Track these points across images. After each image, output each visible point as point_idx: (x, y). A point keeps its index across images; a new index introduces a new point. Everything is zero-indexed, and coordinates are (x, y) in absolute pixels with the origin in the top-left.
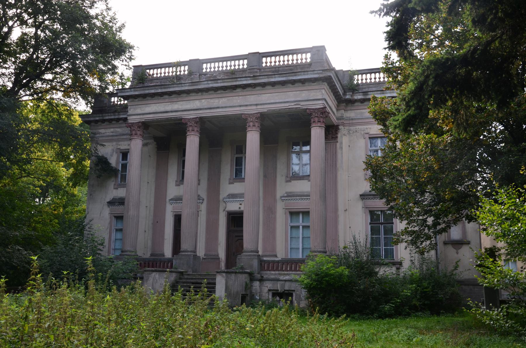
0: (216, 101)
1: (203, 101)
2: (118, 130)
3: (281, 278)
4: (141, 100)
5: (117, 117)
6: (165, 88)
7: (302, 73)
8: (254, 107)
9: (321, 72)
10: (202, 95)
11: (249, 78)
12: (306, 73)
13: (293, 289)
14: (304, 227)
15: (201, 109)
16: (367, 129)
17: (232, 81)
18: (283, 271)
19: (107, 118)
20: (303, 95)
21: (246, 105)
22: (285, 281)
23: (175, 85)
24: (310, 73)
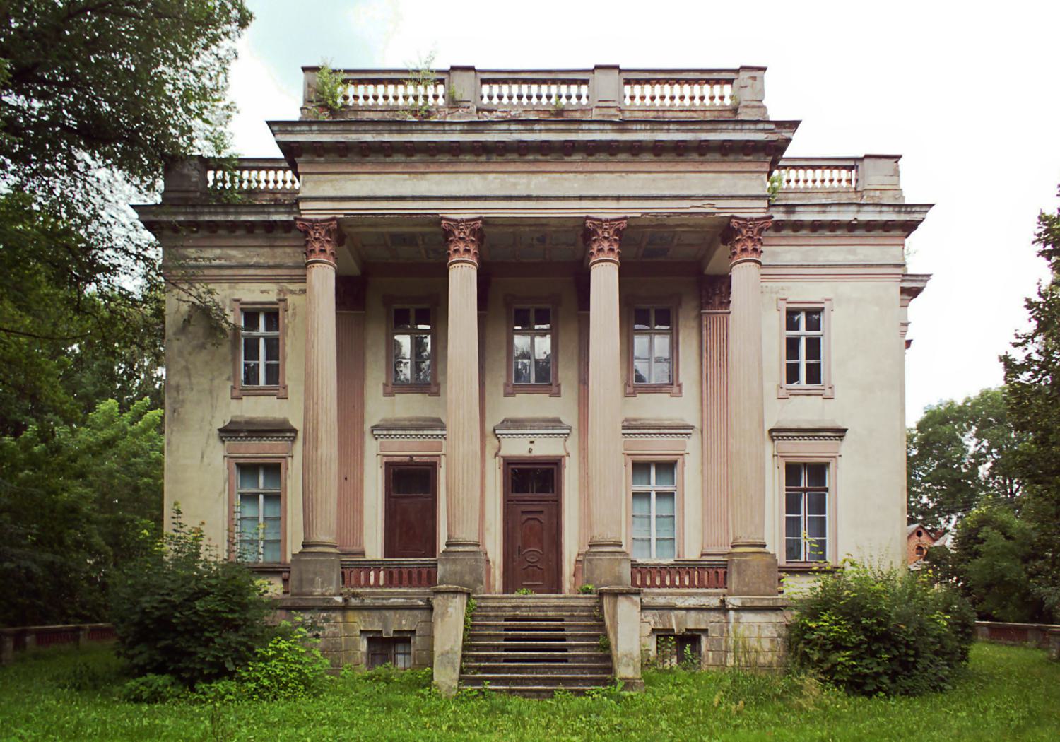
0: (523, 179)
1: (491, 176)
2: (233, 252)
3: (680, 602)
4: (334, 162)
5: (231, 218)
6: (400, 132)
7: (731, 127)
8: (613, 204)
9: (772, 127)
10: (488, 161)
11: (608, 127)
12: (739, 127)
13: (703, 627)
14: (659, 494)
15: (485, 198)
16: (782, 289)
17: (569, 131)
18: (362, 587)
19: (207, 218)
20: (722, 183)
21: (595, 198)
22: (688, 609)
23: (426, 127)
24: (746, 127)
